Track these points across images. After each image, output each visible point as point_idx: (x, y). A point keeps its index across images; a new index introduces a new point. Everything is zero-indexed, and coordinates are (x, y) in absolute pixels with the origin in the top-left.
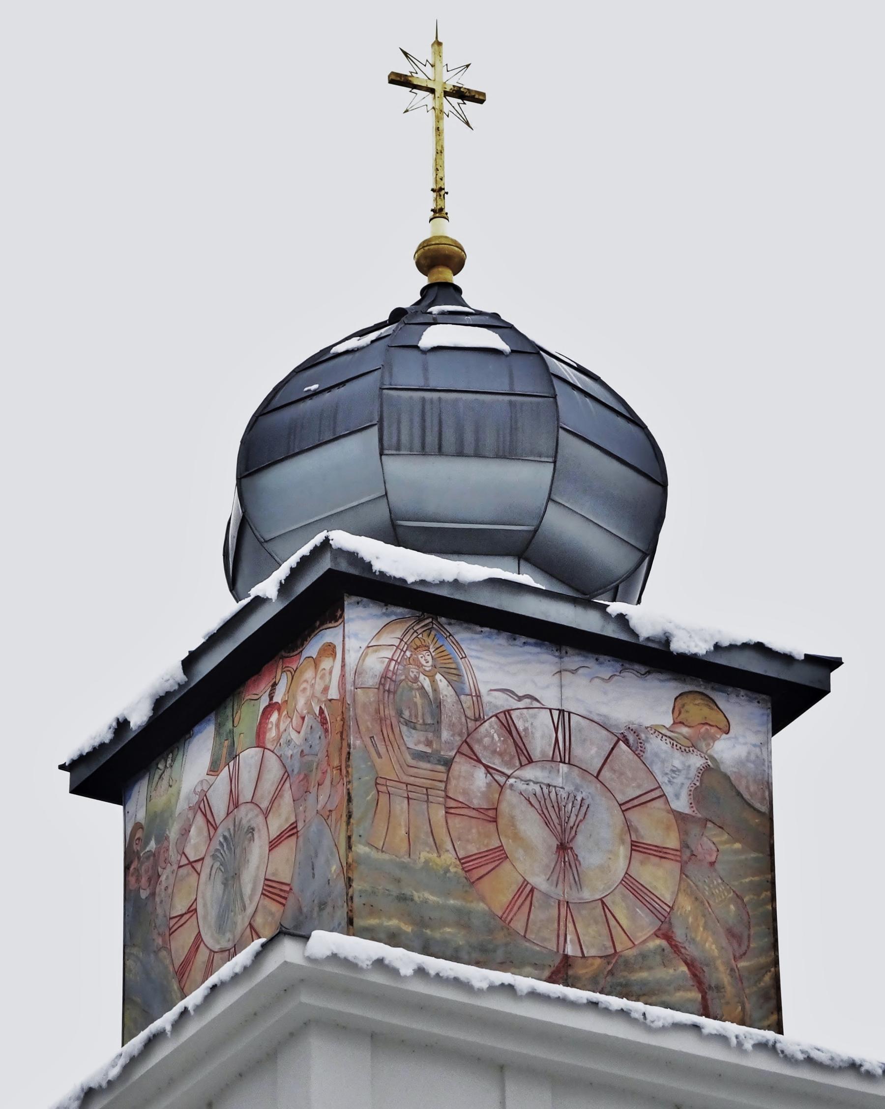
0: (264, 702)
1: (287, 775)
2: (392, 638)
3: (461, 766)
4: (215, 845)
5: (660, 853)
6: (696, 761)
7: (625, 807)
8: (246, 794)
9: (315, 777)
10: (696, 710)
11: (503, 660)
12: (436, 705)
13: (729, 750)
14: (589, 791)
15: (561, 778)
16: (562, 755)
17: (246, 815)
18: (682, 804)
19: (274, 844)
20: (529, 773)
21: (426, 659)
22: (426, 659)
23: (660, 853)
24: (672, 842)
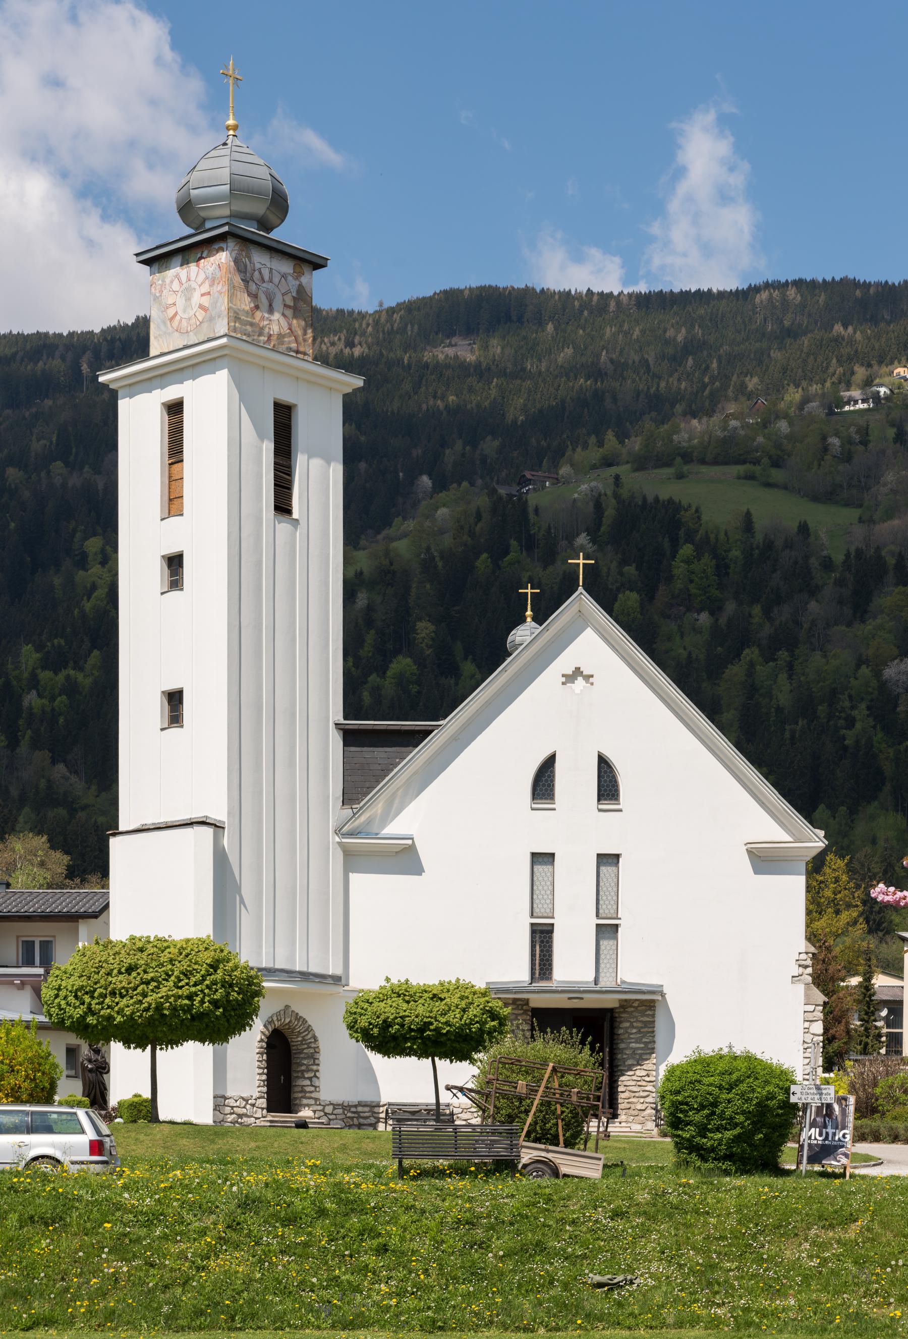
0: (199, 255)
1: (207, 278)
2: (237, 248)
3: (251, 283)
4: (844, 1020)
5: (289, 307)
6: (298, 283)
7: (283, 295)
8: (193, 278)
9: (216, 282)
10: (298, 270)
11: (168, 54)
12: (246, 266)
13: (304, 280)
14: (276, 290)
15: (270, 286)
16: (271, 281)
17: (194, 285)
18: (294, 294)
19: (202, 295)
20: (264, 285)
21: (244, 254)
22: (244, 254)
23: (289, 307)
24: (292, 304)
